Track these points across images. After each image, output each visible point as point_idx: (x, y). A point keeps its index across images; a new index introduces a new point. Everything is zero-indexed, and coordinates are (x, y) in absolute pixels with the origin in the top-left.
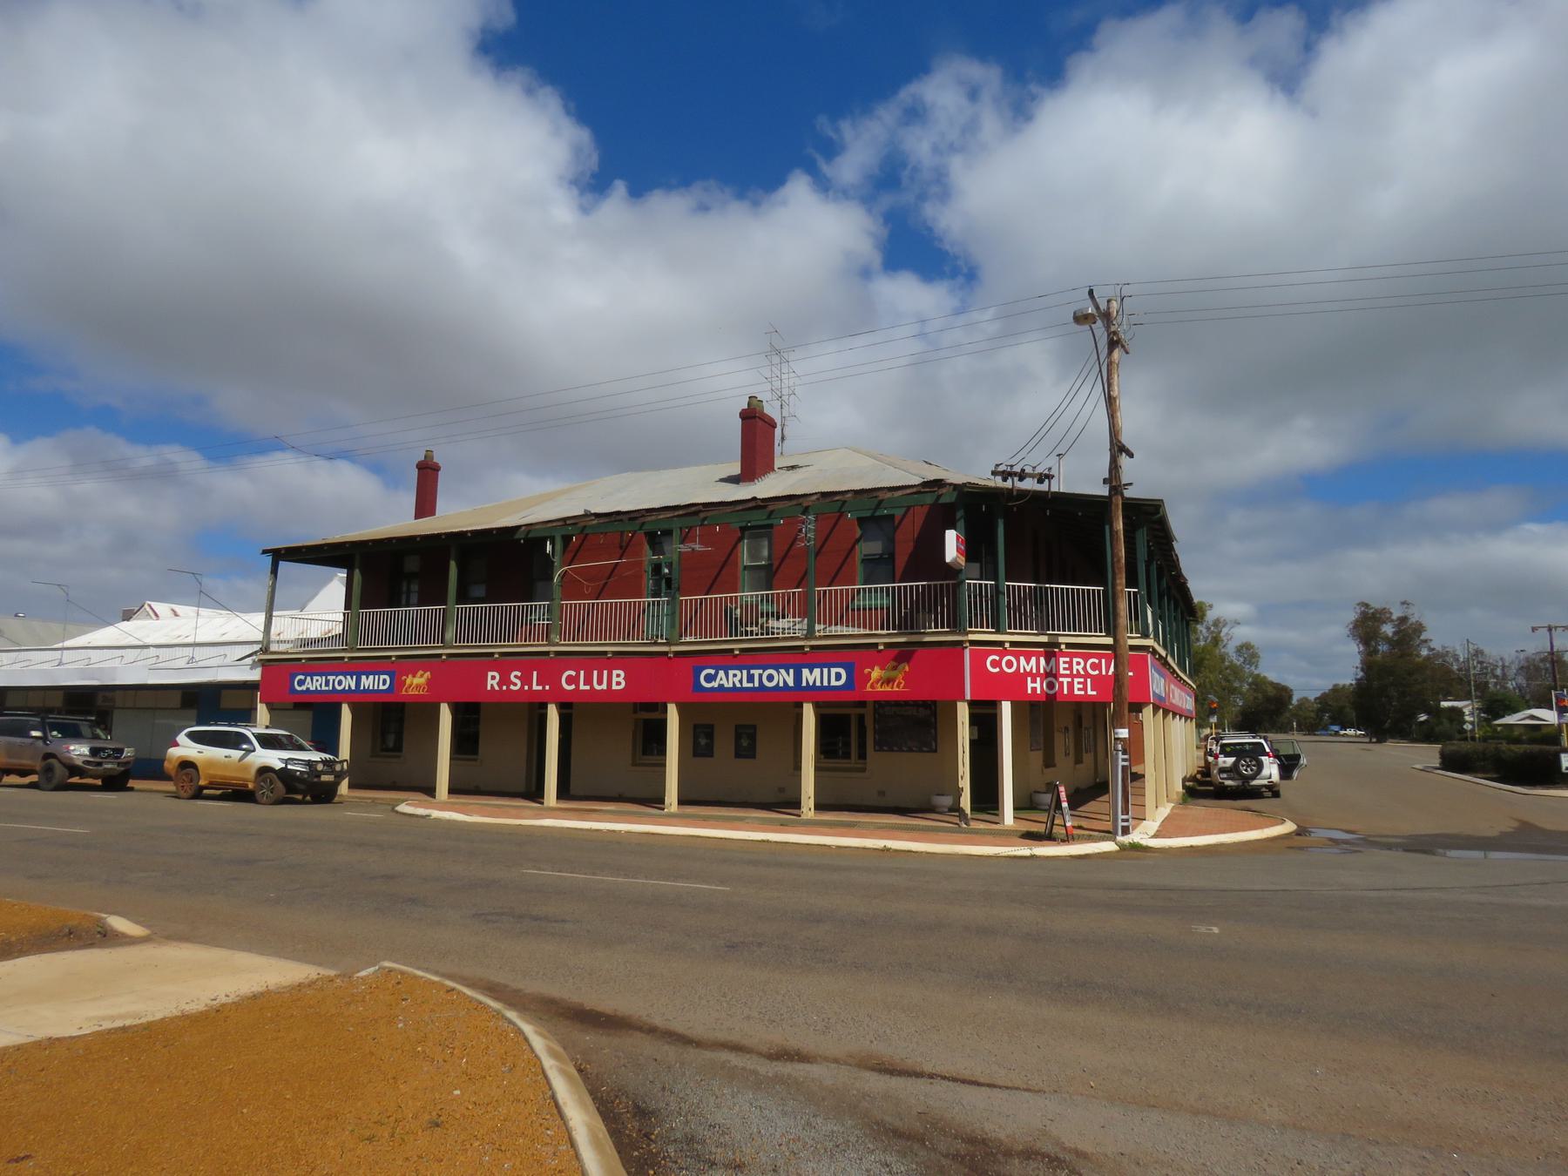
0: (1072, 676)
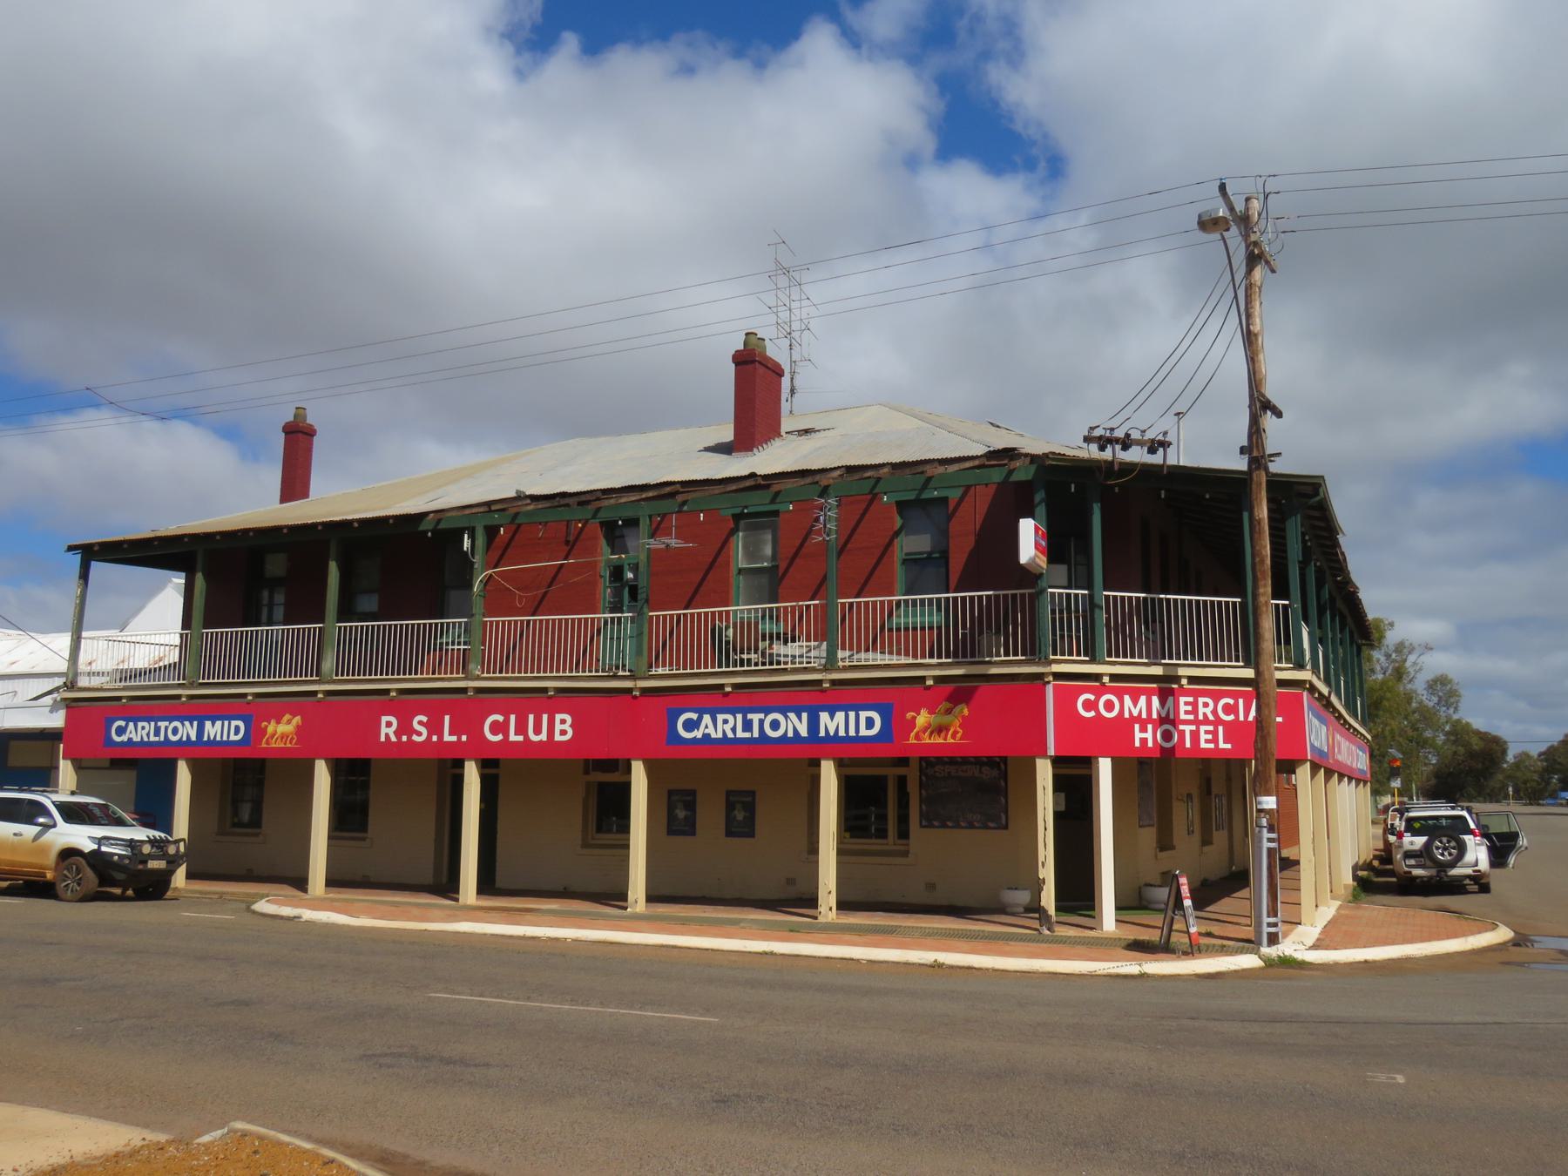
0: (1197, 722)
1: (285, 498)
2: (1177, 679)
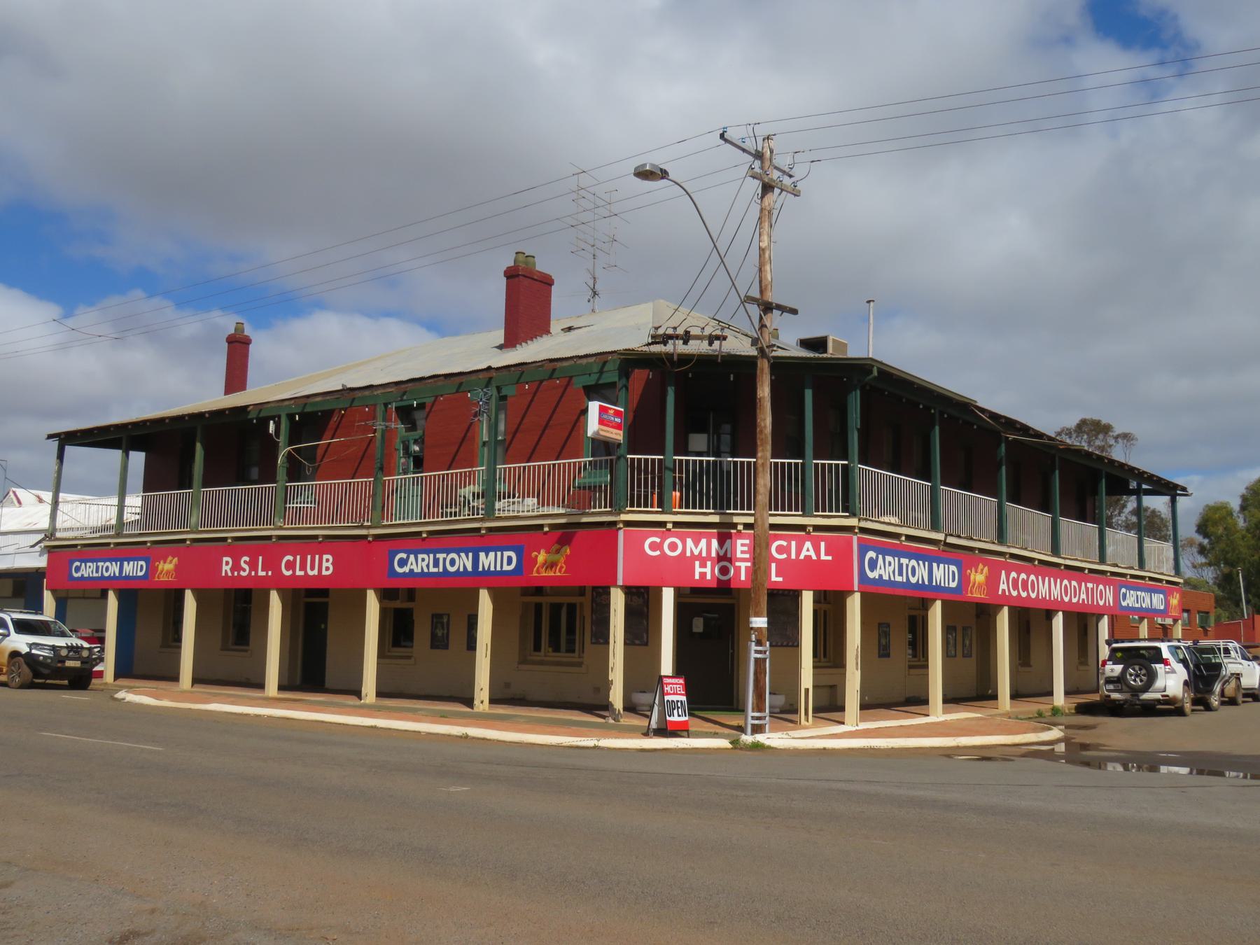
1: (227, 392)
2: (734, 526)
